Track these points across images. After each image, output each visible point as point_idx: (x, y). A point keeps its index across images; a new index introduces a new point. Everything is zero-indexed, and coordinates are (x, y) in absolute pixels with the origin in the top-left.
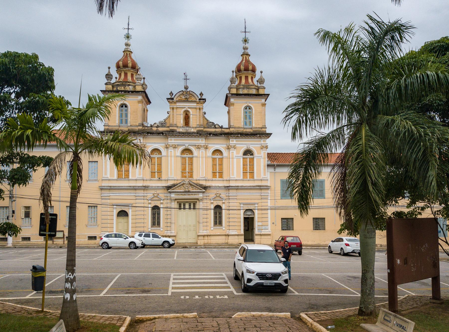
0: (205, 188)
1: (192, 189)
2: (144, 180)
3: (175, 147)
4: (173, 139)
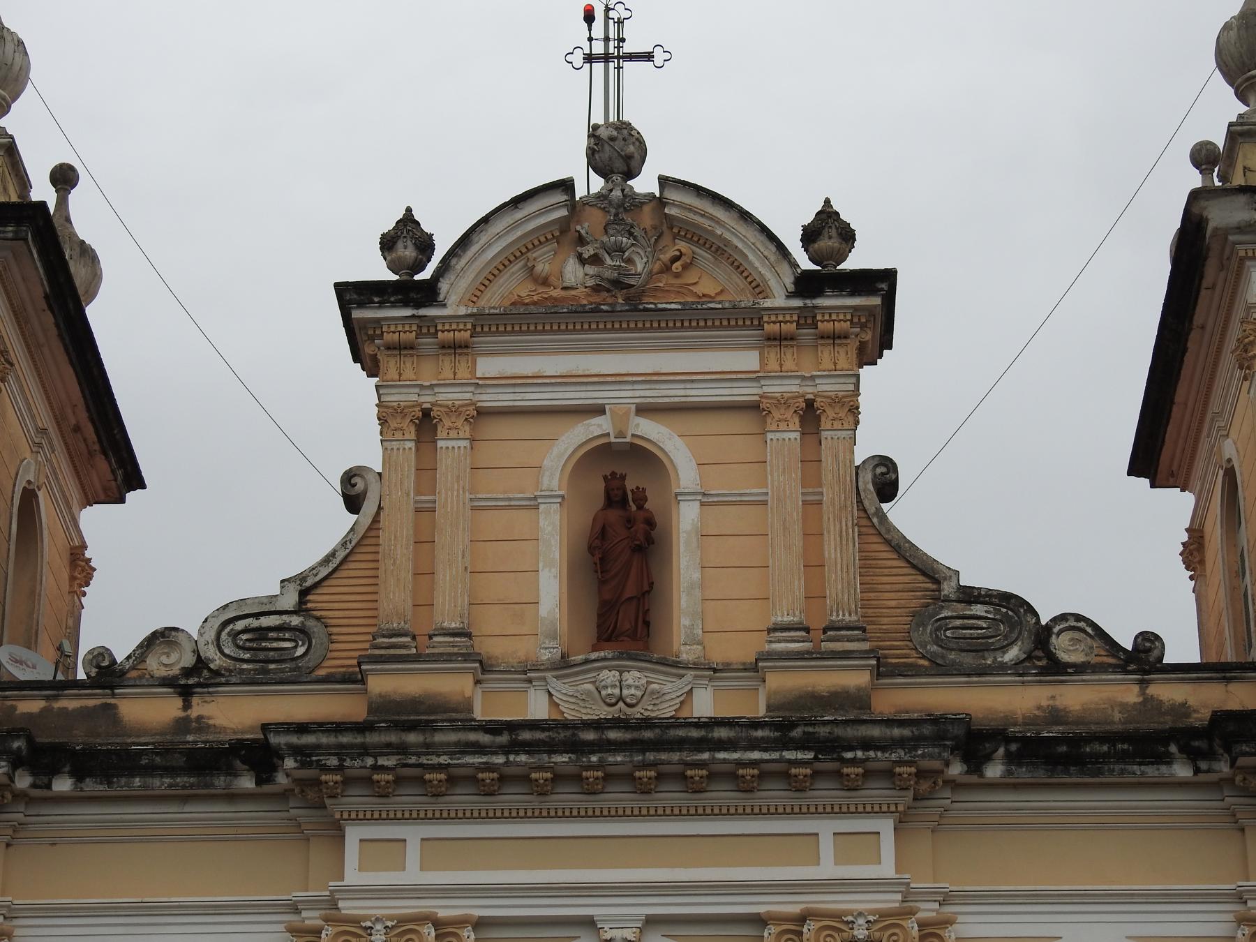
4: (413, 834)
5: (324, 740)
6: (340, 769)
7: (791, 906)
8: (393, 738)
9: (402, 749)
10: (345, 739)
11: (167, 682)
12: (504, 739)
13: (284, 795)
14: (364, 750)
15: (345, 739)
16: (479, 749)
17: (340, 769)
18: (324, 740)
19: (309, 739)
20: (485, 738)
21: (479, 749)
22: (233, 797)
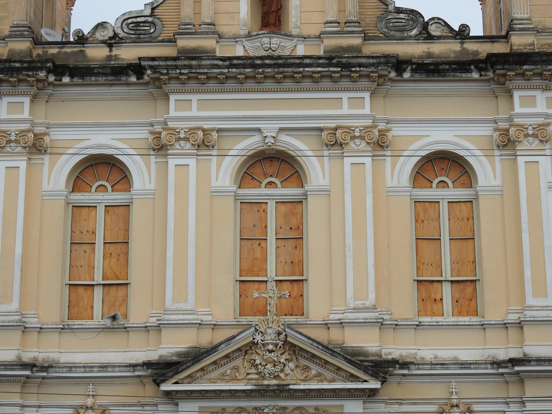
0: (381, 368)
1: (298, 374)
2: (25, 329)
3: (204, 142)
4: (195, 98)
5: (161, 63)
6: (167, 74)
7: (332, 124)
8: (186, 62)
9: (190, 67)
10: (169, 63)
11: (104, 42)
12: (227, 63)
13: (147, 84)
14: (176, 67)
15: (169, 63)
16: (218, 67)
17: (167, 74)
18: (161, 63)
19: (156, 63)
20: (220, 63)
21: (218, 67)
22: (128, 84)
